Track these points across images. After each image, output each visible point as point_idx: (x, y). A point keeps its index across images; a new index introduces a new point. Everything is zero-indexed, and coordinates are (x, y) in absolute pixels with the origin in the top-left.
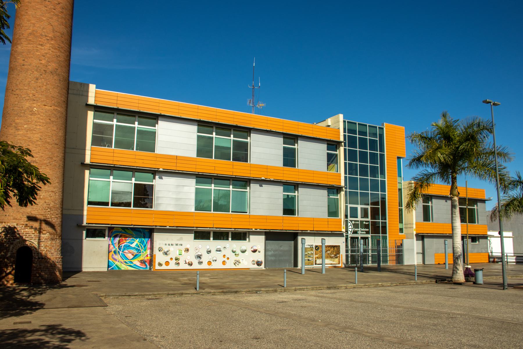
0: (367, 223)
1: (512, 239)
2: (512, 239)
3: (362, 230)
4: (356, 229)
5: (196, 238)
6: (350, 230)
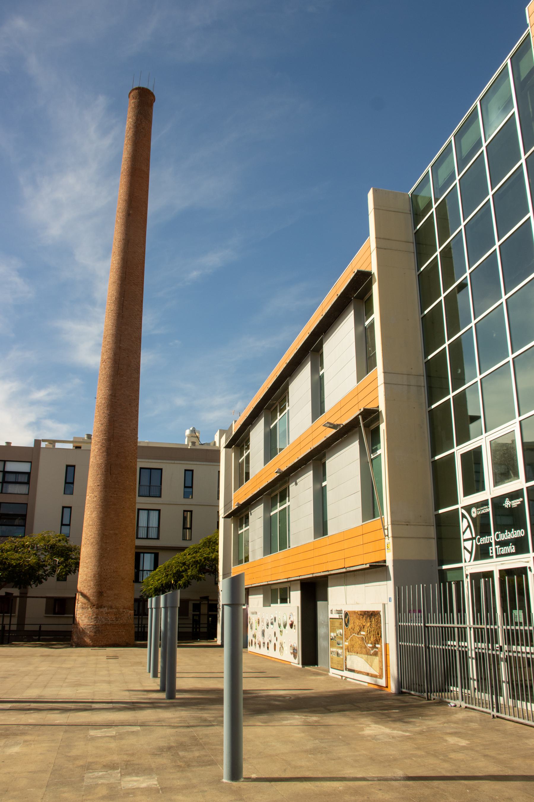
0: (515, 503)
4: (484, 540)
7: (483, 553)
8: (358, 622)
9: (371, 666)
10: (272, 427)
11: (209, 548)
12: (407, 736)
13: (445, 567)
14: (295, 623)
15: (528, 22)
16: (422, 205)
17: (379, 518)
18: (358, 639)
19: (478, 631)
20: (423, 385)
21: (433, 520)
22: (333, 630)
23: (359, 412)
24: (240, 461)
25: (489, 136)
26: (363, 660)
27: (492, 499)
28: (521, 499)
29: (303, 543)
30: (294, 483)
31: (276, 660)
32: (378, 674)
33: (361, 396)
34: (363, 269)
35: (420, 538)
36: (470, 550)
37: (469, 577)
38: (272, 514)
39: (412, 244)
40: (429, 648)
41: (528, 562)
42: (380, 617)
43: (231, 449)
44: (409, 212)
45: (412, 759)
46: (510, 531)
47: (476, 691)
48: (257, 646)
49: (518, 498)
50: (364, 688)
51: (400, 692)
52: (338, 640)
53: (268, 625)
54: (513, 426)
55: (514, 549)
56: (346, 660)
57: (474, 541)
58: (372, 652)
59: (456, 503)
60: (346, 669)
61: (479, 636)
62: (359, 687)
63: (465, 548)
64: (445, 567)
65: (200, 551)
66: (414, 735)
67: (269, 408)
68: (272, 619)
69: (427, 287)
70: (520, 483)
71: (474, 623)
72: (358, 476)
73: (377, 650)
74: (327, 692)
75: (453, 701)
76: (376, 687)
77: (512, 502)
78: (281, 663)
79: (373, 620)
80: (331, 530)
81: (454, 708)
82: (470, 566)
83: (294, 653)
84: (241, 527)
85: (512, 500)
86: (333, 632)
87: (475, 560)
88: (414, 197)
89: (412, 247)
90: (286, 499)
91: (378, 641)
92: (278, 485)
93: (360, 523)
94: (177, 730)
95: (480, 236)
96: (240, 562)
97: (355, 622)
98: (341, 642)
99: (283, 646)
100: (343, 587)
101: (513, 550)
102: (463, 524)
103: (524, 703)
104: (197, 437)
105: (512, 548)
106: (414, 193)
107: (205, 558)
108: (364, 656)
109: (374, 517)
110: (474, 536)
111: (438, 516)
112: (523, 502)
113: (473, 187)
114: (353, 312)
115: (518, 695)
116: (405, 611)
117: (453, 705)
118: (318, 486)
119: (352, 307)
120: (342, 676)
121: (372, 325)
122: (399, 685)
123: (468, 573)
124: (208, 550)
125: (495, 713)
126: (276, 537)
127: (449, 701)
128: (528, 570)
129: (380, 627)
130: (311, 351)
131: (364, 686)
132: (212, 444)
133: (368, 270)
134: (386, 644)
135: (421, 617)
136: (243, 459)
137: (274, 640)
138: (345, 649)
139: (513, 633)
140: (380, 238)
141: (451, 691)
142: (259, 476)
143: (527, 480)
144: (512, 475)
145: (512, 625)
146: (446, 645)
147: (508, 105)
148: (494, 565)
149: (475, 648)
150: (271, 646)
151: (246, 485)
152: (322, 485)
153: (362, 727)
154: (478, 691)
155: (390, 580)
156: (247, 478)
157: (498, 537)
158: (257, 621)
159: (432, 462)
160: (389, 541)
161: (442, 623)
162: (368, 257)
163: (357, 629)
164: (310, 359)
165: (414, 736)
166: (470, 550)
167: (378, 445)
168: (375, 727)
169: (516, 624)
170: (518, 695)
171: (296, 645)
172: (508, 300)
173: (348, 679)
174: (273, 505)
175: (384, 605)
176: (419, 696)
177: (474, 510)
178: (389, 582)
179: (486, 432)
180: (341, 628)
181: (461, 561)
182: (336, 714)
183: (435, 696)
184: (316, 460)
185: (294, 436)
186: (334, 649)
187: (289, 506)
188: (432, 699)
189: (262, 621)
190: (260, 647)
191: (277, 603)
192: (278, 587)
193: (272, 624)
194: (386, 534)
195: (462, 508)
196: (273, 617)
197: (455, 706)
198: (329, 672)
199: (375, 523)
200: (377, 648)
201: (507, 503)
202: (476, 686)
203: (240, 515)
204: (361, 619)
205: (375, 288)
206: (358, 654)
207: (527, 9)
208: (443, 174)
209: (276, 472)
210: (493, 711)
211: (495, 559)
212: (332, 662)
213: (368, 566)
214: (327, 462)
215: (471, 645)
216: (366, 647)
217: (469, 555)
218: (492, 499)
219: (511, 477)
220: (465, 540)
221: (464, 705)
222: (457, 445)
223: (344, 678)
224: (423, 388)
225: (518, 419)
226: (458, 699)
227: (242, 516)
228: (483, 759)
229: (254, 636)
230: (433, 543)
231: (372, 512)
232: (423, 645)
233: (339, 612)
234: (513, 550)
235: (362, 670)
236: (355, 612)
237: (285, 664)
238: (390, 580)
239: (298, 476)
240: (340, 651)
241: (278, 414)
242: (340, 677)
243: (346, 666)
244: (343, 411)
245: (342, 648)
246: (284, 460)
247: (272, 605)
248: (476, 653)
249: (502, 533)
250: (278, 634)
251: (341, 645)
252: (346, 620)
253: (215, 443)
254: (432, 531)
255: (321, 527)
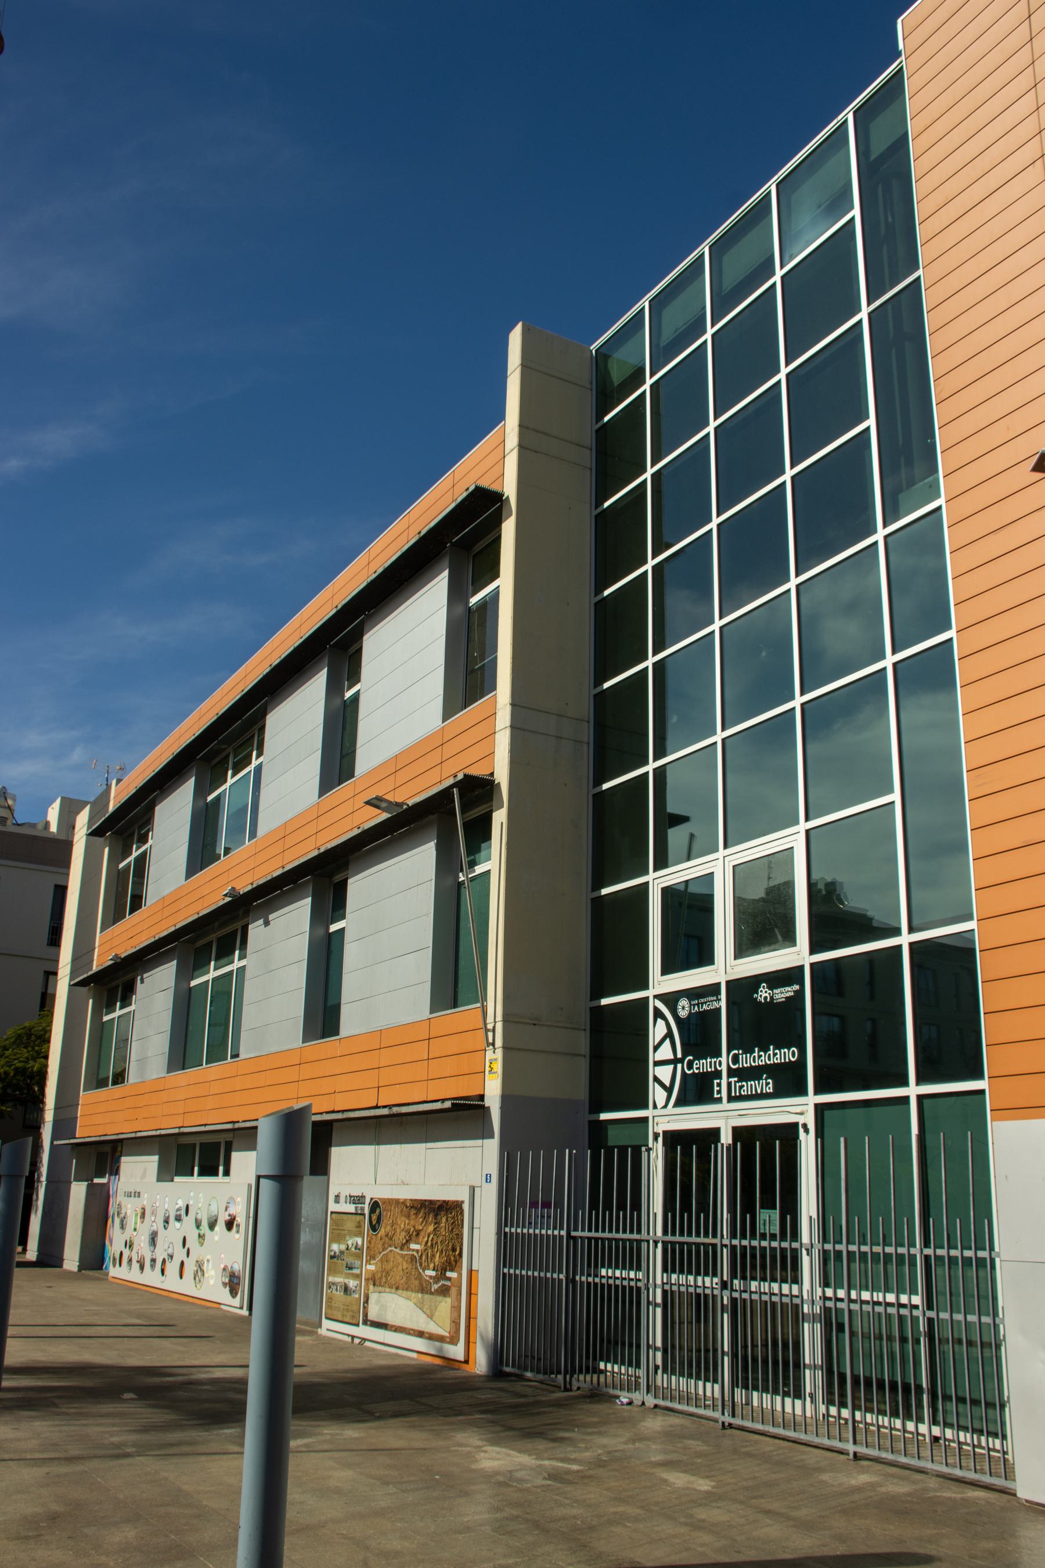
0: (782, 994)
1: (296, 1363)
2: (296, 1363)
3: (747, 1061)
4: (703, 1065)
5: (165, 1174)
6: (664, 1073)
7: (697, 1090)
8: (402, 1223)
9: (431, 1317)
10: (210, 798)
11: (26, 1047)
12: (578, 1471)
13: (604, 1116)
14: (240, 1220)
15: (901, 47)
16: (617, 376)
17: (479, 1005)
18: (400, 1260)
19: (673, 1251)
20: (585, 739)
21: (585, 1019)
22: (338, 1238)
23: (451, 781)
24: (121, 866)
25: (792, 258)
26: (411, 1304)
27: (728, 982)
28: (796, 987)
29: (274, 1049)
30: (261, 921)
31: (195, 1301)
32: (447, 1334)
33: (450, 749)
34: (485, 483)
35: (557, 1053)
36: (668, 1084)
37: (660, 1139)
38: (193, 983)
39: (588, 451)
40: (574, 1281)
41: (802, 1114)
42: (462, 1213)
43: (101, 840)
44: (588, 385)
45: (626, 1526)
46: (766, 1050)
47: (660, 1372)
48: (136, 1266)
49: (789, 985)
50: (413, 1362)
51: (497, 1372)
52: (350, 1260)
53: (166, 1221)
54: (793, 839)
55: (771, 1085)
56: (367, 1301)
57: (679, 1066)
58: (435, 1287)
59: (645, 986)
60: (365, 1322)
61: (677, 1259)
62: (396, 1362)
63: (656, 1079)
64: (604, 1116)
65: (7, 1053)
66: (590, 1469)
67: (207, 759)
68: (178, 1210)
69: (615, 540)
70: (798, 954)
71: (665, 1232)
72: (427, 915)
73: (448, 1283)
74: (337, 1371)
75: (625, 1393)
76: (438, 1361)
77: (775, 991)
78: (193, 1304)
79: (444, 1219)
80: (350, 1022)
81: (629, 1407)
82: (665, 1115)
83: (233, 1284)
84: (111, 1008)
85: (777, 988)
86: (339, 1242)
87: (676, 1105)
88: (603, 356)
89: (588, 458)
90: (234, 952)
91: (452, 1262)
92: (217, 924)
93: (425, 1012)
94: (44, 1470)
95: (749, 451)
96: (102, 1083)
97: (399, 1224)
98: (357, 1263)
99: (205, 1268)
100: (369, 1149)
101: (770, 1089)
102: (657, 1030)
103: (779, 1399)
104: (9, 807)
105: (767, 1084)
106: (601, 350)
107: (16, 1070)
108: (413, 1295)
109: (455, 1006)
110: (679, 1055)
111: (598, 1012)
112: (800, 994)
113: (745, 353)
114: (446, 573)
115: (765, 1380)
116: (522, 1203)
117: (625, 1400)
118: (320, 932)
119: (446, 562)
120: (353, 1337)
121: (491, 604)
122: (497, 1356)
123: (660, 1130)
124: (25, 1053)
125: (727, 1419)
126: (203, 1032)
127: (617, 1392)
128: (801, 1130)
129: (460, 1236)
130: (336, 647)
131: (413, 1359)
132: (40, 827)
133: (495, 487)
134: (471, 1271)
135: (549, 1217)
136: (129, 864)
137: (180, 1254)
138: (367, 1280)
139: (753, 1256)
140: (527, 428)
141: (601, 1372)
142: (166, 903)
143: (812, 951)
144: (779, 937)
145: (753, 1236)
146: (596, 1276)
147: (840, 202)
148: (722, 1118)
149: (663, 1284)
150: (172, 1268)
151: (130, 920)
152: (328, 928)
153: (470, 1452)
154: (665, 1371)
155: (493, 1137)
156: (137, 902)
157: (736, 1059)
158: (139, 1211)
159: (592, 899)
160: (495, 1057)
161: (610, 1231)
162: (498, 459)
163: (401, 1237)
164: (326, 661)
165: (591, 1472)
166: (668, 1084)
167: (477, 856)
168: (498, 1453)
169: (763, 1236)
170: (755, 1379)
171: (237, 1267)
172: (801, 587)
173: (367, 1344)
174: (200, 964)
175: (473, 1189)
176: (541, 1382)
177: (684, 1002)
178: (487, 1142)
179: (726, 847)
180: (360, 1234)
181: (645, 1106)
182: (392, 1422)
183: (583, 1381)
184: (325, 878)
185: (271, 818)
186: (338, 1279)
187: (242, 970)
188: (575, 1388)
189: (153, 1213)
190: (142, 1268)
191: (217, 1174)
192: (198, 1140)
193: (178, 1219)
194: (491, 1041)
195: (655, 997)
196: (181, 1203)
197: (630, 1403)
198: (320, 1326)
199: (465, 1015)
200: (449, 1279)
201: (763, 993)
202: (659, 1362)
203: (114, 983)
204: (413, 1217)
205: (509, 529)
206: (400, 1292)
207: (899, 21)
208: (675, 318)
209: (225, 895)
210: (723, 1414)
211: (725, 1105)
212: (329, 1307)
213: (448, 1104)
214: (350, 881)
215: (656, 1278)
216: (419, 1277)
217: (665, 1094)
218: (728, 982)
219: (776, 942)
220: (657, 1063)
221: (650, 1401)
222: (655, 870)
223: (357, 1341)
224: (585, 747)
225: (803, 826)
226: (637, 1387)
227: (114, 984)
228: (770, 1522)
229: (129, 1245)
230: (583, 1067)
231: (451, 992)
232: (562, 1276)
233: (358, 1200)
234: (770, 1089)
235: (408, 1325)
236: (397, 1202)
237: (208, 1308)
238: (493, 1137)
239: (273, 905)
240: (352, 1283)
241: (230, 773)
242: (349, 1339)
243: (366, 1315)
244: (402, 777)
245: (358, 1277)
246: (241, 869)
247: (177, 1179)
248: (665, 1293)
249: (745, 1052)
250: (192, 1242)
251: (356, 1271)
252: (374, 1217)
253: (47, 824)
254: (583, 1042)
255: (323, 1015)
